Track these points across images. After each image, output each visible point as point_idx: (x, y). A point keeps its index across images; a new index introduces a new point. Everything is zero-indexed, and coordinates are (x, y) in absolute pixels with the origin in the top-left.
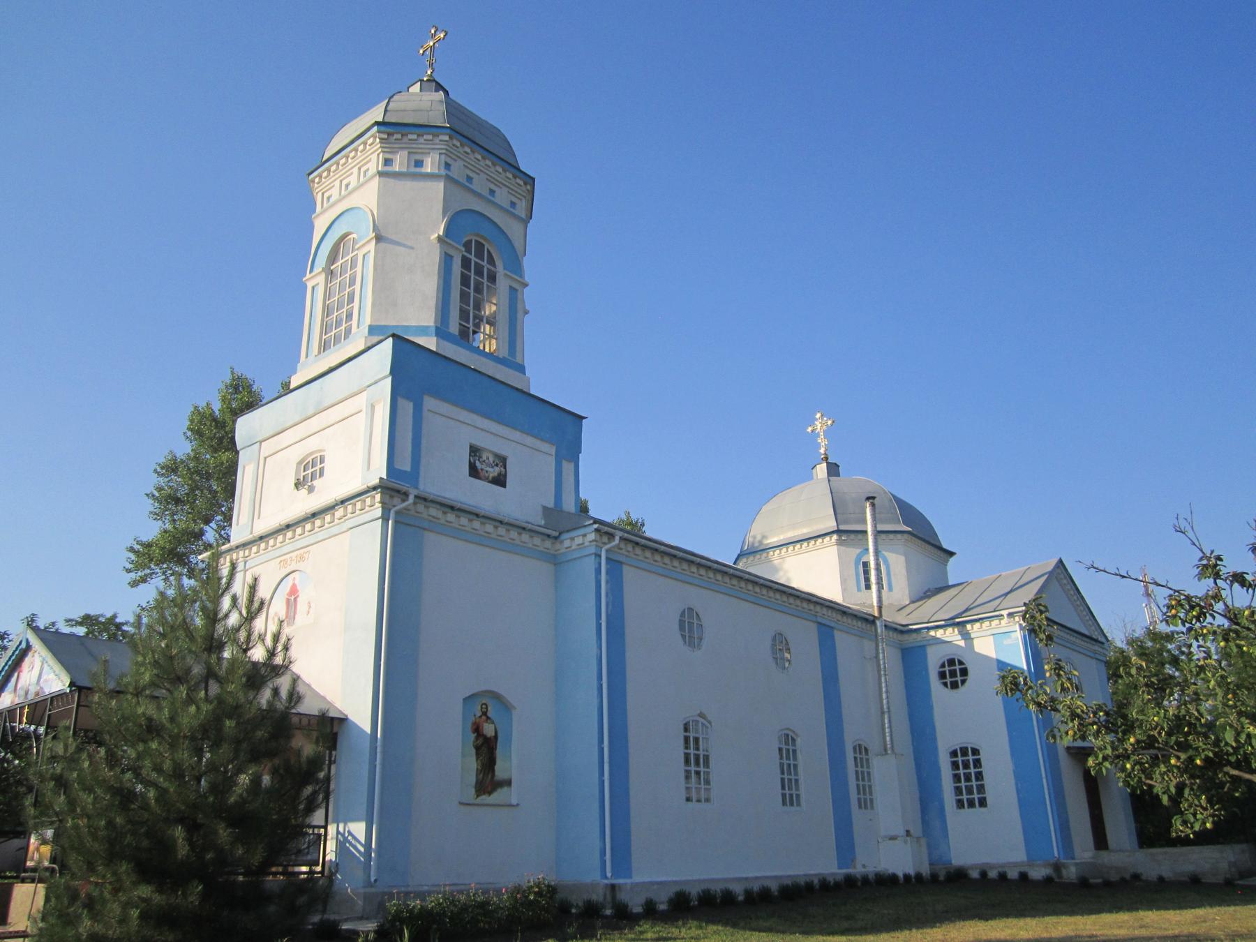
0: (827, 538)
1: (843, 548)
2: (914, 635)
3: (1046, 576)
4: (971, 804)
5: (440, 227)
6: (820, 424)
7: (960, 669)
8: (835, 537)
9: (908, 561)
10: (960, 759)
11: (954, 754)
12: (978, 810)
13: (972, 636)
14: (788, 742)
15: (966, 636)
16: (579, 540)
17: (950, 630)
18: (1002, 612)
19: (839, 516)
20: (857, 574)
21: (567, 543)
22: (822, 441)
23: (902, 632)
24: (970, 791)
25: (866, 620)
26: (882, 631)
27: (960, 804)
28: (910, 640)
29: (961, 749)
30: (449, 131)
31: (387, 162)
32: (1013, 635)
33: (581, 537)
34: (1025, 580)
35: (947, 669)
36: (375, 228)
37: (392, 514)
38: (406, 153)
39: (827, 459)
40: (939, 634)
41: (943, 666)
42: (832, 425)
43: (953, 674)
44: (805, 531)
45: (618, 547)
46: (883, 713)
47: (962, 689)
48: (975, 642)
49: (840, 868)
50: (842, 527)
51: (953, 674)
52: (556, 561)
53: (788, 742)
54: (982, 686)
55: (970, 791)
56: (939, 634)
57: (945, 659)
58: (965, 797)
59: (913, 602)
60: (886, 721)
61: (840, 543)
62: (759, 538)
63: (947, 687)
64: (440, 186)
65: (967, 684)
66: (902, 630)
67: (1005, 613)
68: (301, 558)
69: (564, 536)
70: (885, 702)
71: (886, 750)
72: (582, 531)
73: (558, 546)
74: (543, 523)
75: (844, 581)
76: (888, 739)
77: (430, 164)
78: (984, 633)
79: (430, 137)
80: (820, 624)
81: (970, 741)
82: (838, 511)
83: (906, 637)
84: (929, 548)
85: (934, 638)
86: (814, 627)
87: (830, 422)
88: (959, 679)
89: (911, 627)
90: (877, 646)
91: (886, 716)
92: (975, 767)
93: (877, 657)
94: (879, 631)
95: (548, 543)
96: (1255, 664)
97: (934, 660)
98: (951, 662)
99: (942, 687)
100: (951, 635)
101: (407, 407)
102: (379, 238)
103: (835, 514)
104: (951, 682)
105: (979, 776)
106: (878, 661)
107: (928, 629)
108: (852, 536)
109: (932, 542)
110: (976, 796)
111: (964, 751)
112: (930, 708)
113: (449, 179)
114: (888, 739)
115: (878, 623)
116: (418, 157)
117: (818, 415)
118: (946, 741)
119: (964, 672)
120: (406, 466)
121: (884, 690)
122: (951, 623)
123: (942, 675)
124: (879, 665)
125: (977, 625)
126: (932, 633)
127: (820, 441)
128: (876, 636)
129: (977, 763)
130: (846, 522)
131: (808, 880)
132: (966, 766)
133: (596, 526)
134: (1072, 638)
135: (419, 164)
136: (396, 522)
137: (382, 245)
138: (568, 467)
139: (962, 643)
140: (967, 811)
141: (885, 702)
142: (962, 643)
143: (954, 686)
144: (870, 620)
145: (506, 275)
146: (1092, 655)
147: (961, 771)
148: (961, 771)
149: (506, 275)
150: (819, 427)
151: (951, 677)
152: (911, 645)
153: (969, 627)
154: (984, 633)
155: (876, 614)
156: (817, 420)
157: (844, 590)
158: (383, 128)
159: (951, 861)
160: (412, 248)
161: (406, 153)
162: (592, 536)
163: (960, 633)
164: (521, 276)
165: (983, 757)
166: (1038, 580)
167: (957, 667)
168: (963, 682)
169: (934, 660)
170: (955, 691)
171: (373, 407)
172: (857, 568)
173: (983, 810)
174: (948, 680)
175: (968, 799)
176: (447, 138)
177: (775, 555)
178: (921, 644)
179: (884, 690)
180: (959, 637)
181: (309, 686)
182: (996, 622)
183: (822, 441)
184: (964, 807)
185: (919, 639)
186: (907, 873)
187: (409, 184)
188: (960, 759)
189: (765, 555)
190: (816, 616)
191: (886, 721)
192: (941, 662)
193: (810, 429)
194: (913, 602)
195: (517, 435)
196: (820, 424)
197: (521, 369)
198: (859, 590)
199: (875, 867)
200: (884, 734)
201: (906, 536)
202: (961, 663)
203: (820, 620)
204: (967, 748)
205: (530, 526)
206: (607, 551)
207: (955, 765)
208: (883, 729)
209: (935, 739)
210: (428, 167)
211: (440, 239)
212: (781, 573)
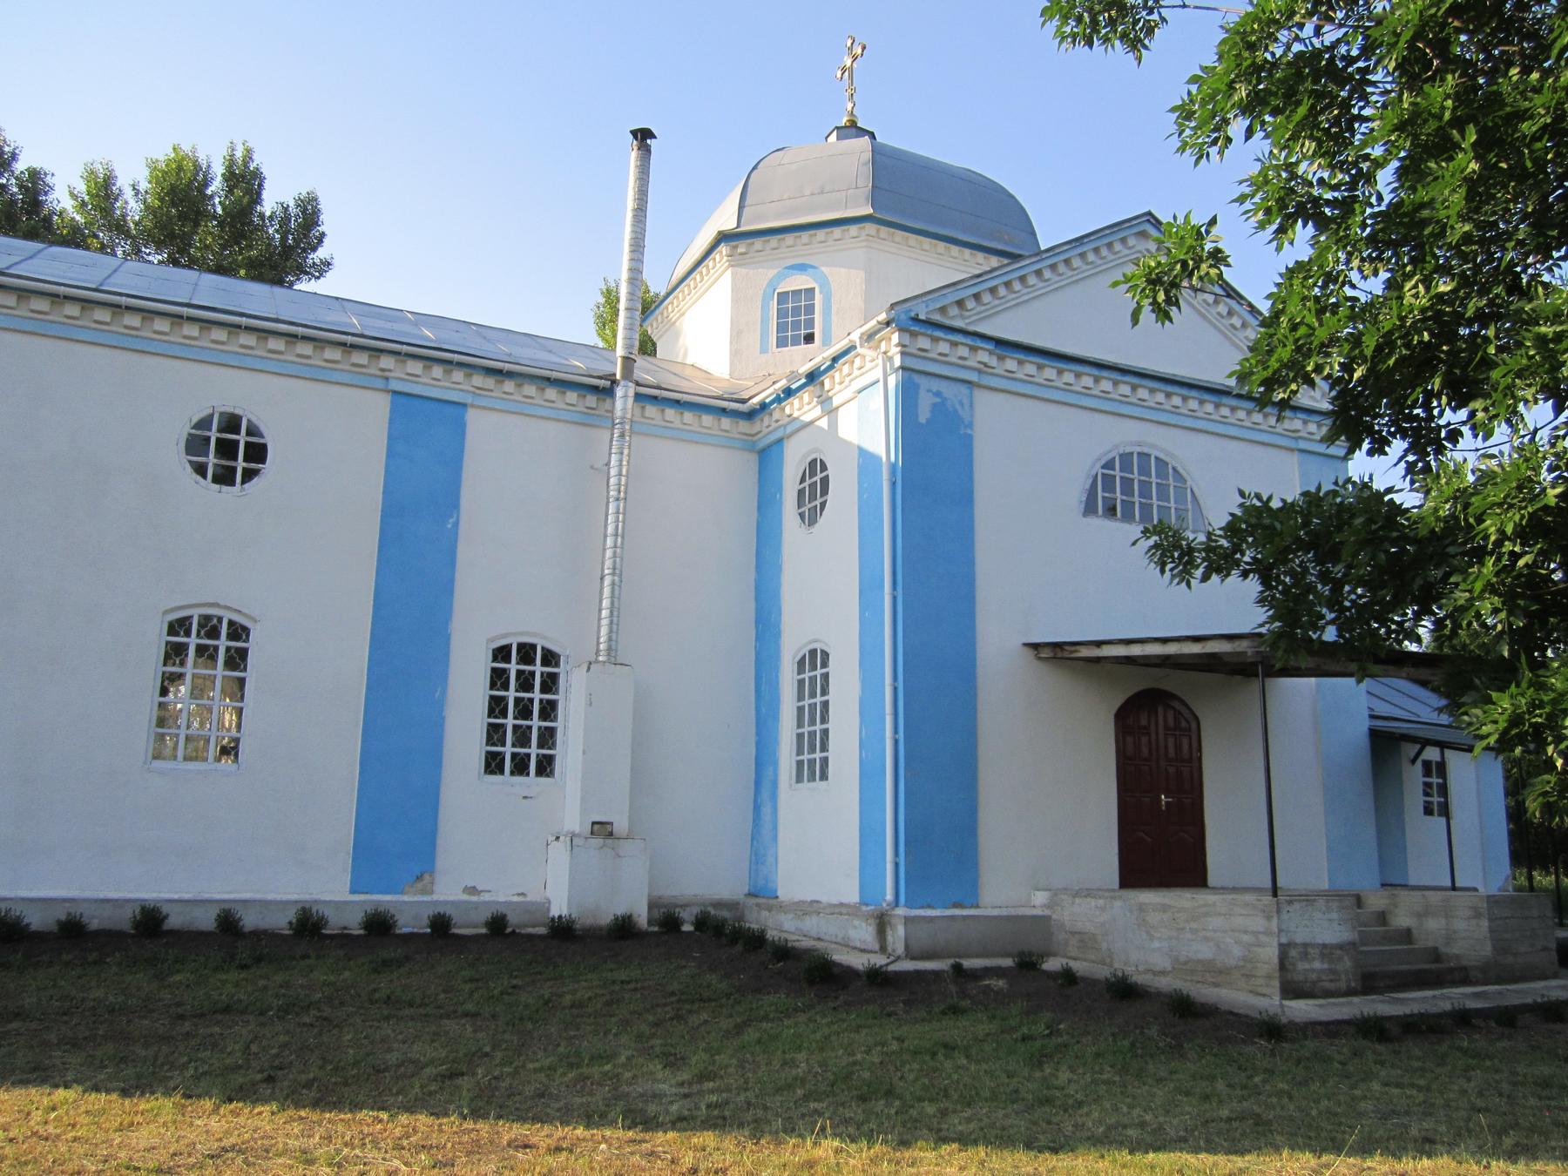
1: (742, 271)
4: (520, 766)
10: (513, 667)
12: (532, 781)
19: (746, 211)
20: (765, 320)
24: (522, 737)
26: (624, 409)
27: (493, 764)
33: (1245, 412)
49: (353, 892)
55: (522, 737)
61: (735, 261)
63: (204, 476)
75: (737, 334)
80: (395, 393)
84: (1267, 696)
92: (541, 745)
110: (534, 751)
111: (527, 652)
129: (550, 683)
131: (72, 911)
134: (388, 325)
140: (506, 781)
146: (1292, 444)
148: (512, 694)
157: (735, 354)
159: (776, 891)
168: (249, 475)
172: (765, 307)
173: (824, 783)
174: (212, 460)
175: (514, 755)
184: (502, 772)
186: (63, 918)
188: (513, 667)
190: (387, 379)
192: (263, 429)
199: (472, 890)
201: (870, 228)
203: (395, 385)
204: (533, 647)
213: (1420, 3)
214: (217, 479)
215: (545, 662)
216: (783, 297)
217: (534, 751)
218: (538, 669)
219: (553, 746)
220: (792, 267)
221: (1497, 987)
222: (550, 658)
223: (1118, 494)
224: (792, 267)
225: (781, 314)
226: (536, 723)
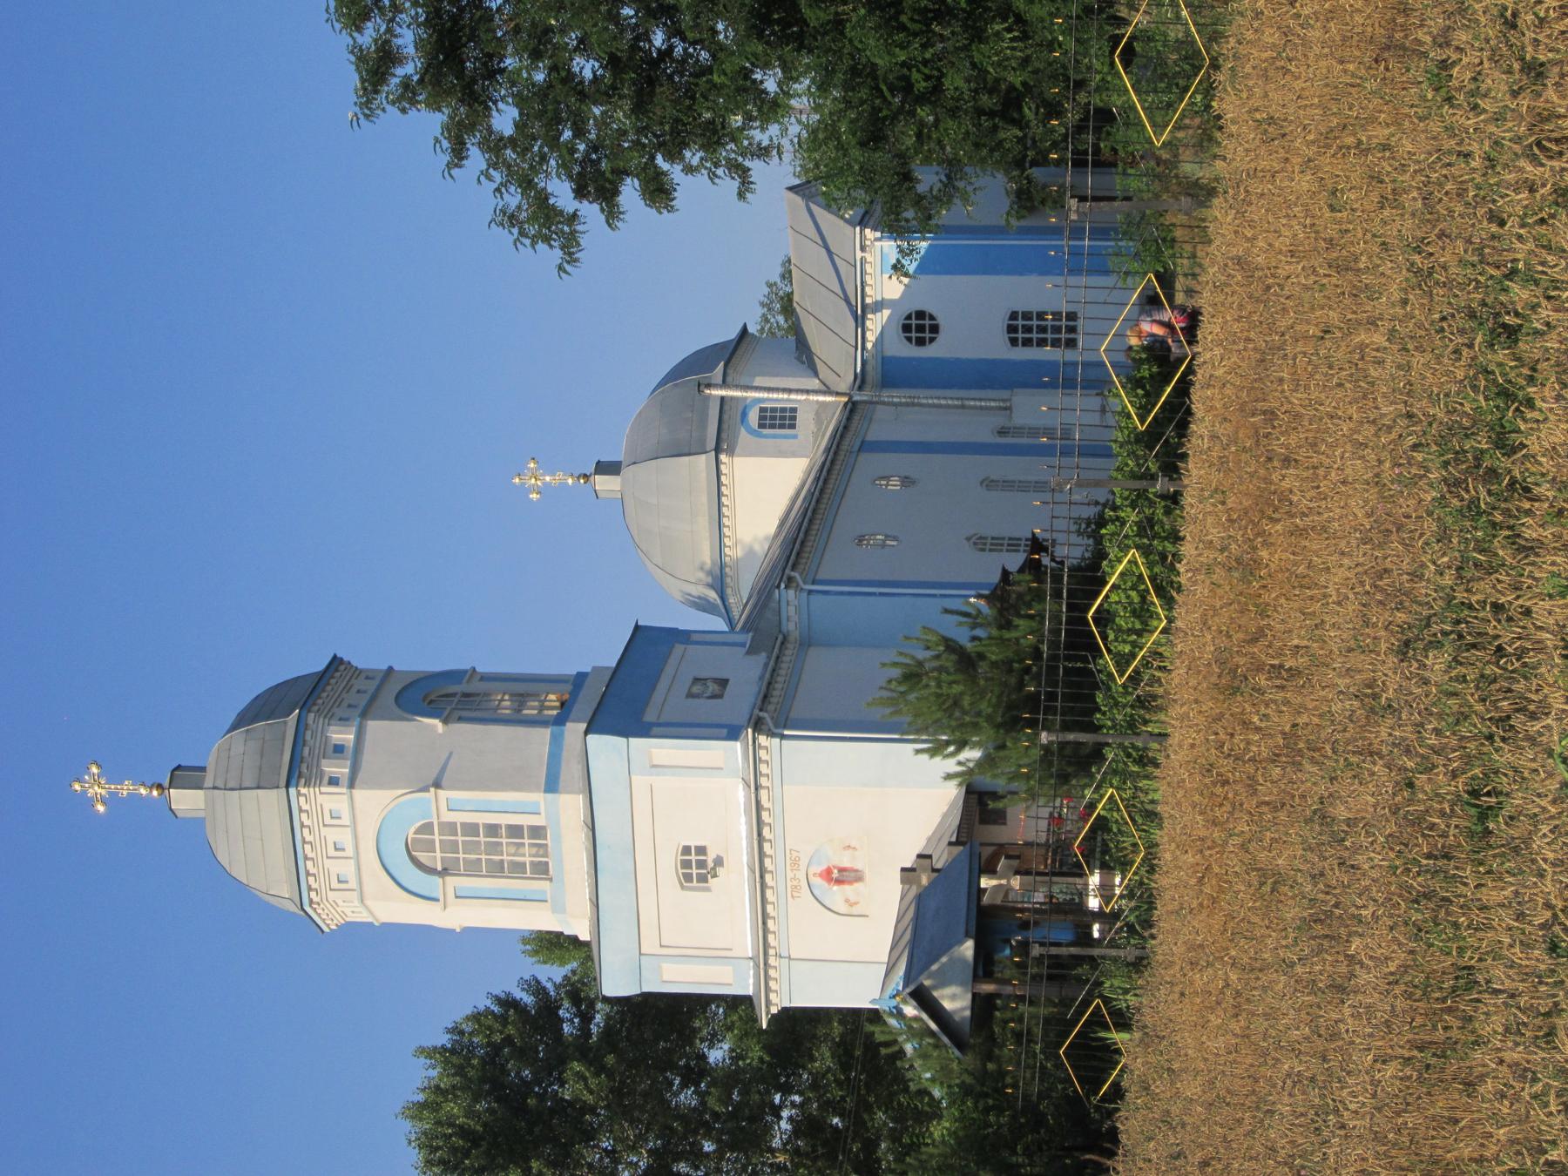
0: (723, 467)
1: (738, 450)
2: (869, 368)
3: (813, 206)
5: (428, 725)
6: (95, 788)
7: (917, 319)
8: (723, 457)
9: (374, 718)
11: (1014, 342)
13: (879, 298)
14: (989, 484)
15: (879, 306)
16: (792, 610)
17: (868, 323)
18: (858, 258)
20: (775, 436)
21: (791, 626)
22: (126, 789)
23: (863, 381)
25: (852, 411)
27: (1071, 343)
28: (872, 374)
29: (1009, 332)
30: (304, 712)
31: (334, 782)
32: (886, 250)
34: (813, 233)
35: (913, 335)
36: (425, 789)
37: (779, 731)
38: (324, 762)
39: (586, 476)
40: (871, 337)
41: (909, 339)
42: (99, 766)
43: (920, 329)
44: (704, 500)
45: (801, 574)
46: (963, 407)
47: (941, 321)
48: (887, 296)
50: (711, 443)
51: (920, 329)
52: (806, 643)
53: (989, 484)
54: (945, 296)
56: (871, 337)
57: (903, 335)
58: (1063, 336)
59: (816, 374)
60: (972, 403)
61: (731, 452)
62: (701, 575)
64: (373, 726)
65: (934, 314)
66: (861, 381)
67: (859, 254)
68: (796, 862)
69: (784, 629)
70: (950, 402)
71: (1005, 409)
72: (783, 604)
73: (791, 638)
74: (764, 655)
75: (781, 454)
76: (993, 404)
77: (343, 735)
78: (879, 284)
79: (309, 733)
81: (1000, 323)
82: (686, 451)
83: (869, 378)
84: (739, 352)
85: (874, 345)
86: (863, 457)
87: (94, 770)
88: (927, 322)
89: (859, 370)
90: (884, 403)
91: (967, 403)
92: (1031, 319)
93: (896, 405)
94: (865, 398)
95: (790, 646)
96: (1566, 324)
97: (903, 349)
98: (906, 328)
99: (934, 344)
100: (875, 324)
101: (655, 730)
102: (437, 785)
103: (689, 454)
104: (930, 332)
105: (1041, 316)
106: (900, 404)
107: (864, 348)
108: (724, 436)
109: (731, 348)
111: (1012, 329)
112: (958, 361)
113: (365, 715)
114: (993, 404)
115: (856, 398)
116: (330, 749)
117: (77, 787)
118: (998, 348)
119: (920, 315)
120: (725, 731)
121: (936, 401)
122: (860, 321)
123: (921, 342)
124: (907, 404)
125: (868, 290)
126: (869, 346)
127: (125, 793)
128: (871, 403)
129: (1027, 316)
130: (703, 441)
132: (1028, 329)
133: (783, 586)
135: (339, 749)
136: (785, 727)
137: (444, 783)
138: (695, 637)
139: (886, 313)
141: (950, 402)
142: (886, 313)
143: (935, 329)
144: (852, 408)
145: (468, 682)
147: (1034, 336)
149: (468, 682)
150: (99, 791)
151: (924, 332)
152: (879, 376)
153: (868, 301)
154: (879, 284)
155: (845, 399)
156: (84, 792)
157: (794, 455)
158: (294, 781)
160: (451, 754)
161: (324, 762)
162: (791, 592)
163: (874, 312)
164: (465, 672)
165: (1020, 307)
166: (815, 213)
167: (914, 322)
168: (932, 318)
169: (903, 349)
170: (941, 328)
171: (654, 766)
172: (765, 436)
174: (927, 335)
176: (312, 715)
177: (733, 552)
178: (880, 360)
179: (936, 401)
180: (879, 314)
181: (929, 840)
182: (868, 268)
183: (126, 789)
185: (874, 362)
187: (367, 757)
189: (727, 570)
191: (972, 403)
192: (905, 341)
193: (101, 808)
194: (816, 374)
195: (669, 671)
196: (95, 788)
197: (580, 678)
198: (795, 437)
200: (987, 408)
201: (730, 371)
202: (909, 317)
205: (768, 675)
206: (805, 583)
207: (1027, 343)
208: (981, 408)
209: (993, 362)
210: (344, 740)
211: (445, 721)
212: (757, 548)
213: (1565, 277)
214: (1009, 326)
215: (1016, 319)
216: (761, 426)
217: (1035, 323)
218: (1020, 322)
219: (1031, 313)
220: (742, 422)
221: (455, 916)
222: (1014, 316)
223: (1064, 243)
224: (742, 422)
225: (772, 426)
226: (1034, 336)
